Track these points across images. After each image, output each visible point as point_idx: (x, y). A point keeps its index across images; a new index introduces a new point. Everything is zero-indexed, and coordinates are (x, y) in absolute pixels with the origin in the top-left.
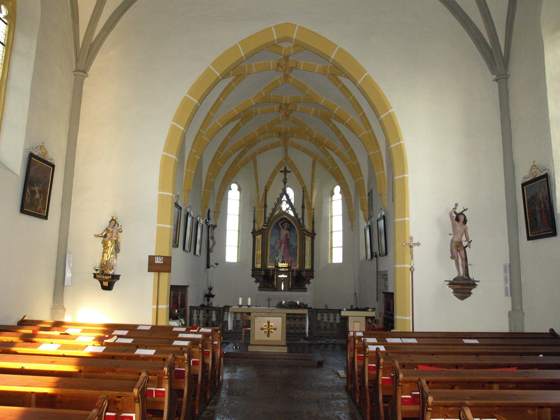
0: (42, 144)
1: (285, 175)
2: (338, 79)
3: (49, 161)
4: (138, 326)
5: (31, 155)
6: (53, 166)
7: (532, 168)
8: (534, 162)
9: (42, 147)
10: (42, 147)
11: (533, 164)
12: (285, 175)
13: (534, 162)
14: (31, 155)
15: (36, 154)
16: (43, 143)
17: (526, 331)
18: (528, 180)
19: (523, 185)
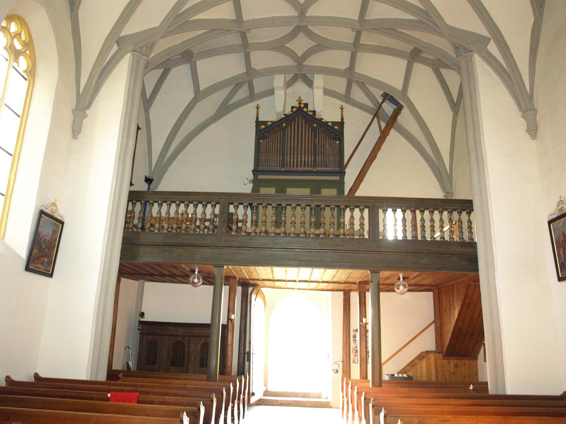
0: (54, 201)
1: (352, 67)
2: (366, 87)
3: (59, 218)
4: (366, 317)
5: (42, 213)
6: (62, 223)
7: (559, 202)
8: (560, 197)
9: (54, 204)
10: (54, 204)
11: (559, 200)
12: (352, 67)
13: (560, 197)
14: (42, 213)
15: (46, 211)
16: (56, 200)
17: (510, 391)
18: (554, 217)
19: (550, 222)
